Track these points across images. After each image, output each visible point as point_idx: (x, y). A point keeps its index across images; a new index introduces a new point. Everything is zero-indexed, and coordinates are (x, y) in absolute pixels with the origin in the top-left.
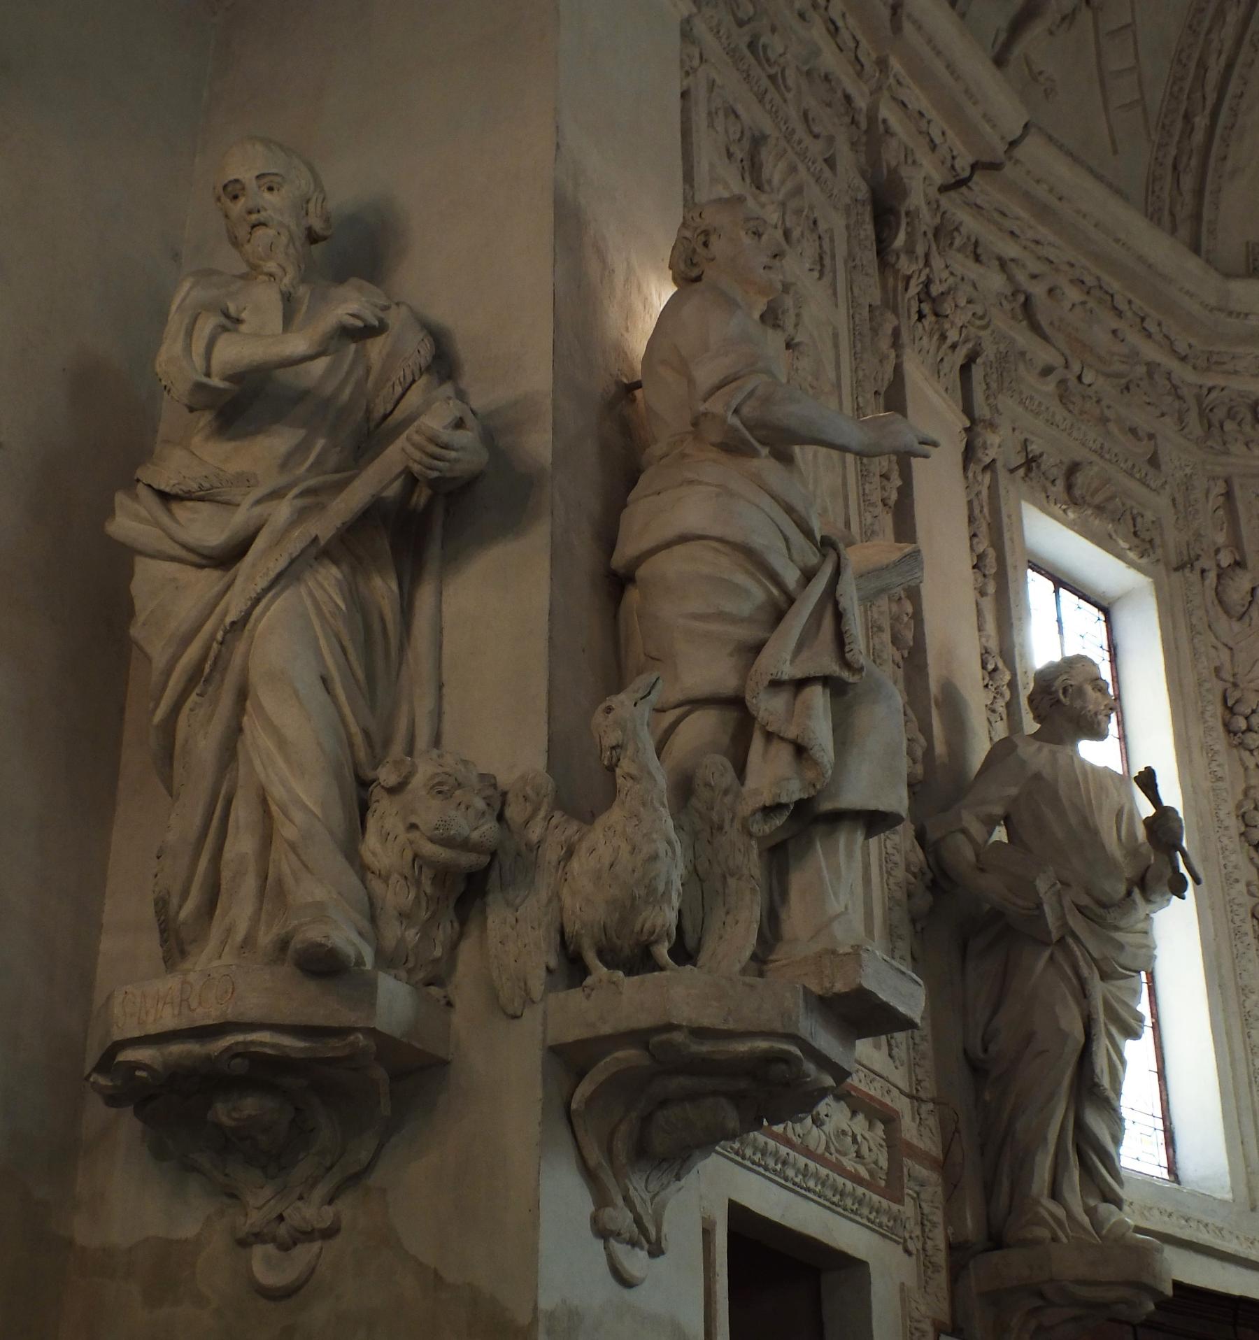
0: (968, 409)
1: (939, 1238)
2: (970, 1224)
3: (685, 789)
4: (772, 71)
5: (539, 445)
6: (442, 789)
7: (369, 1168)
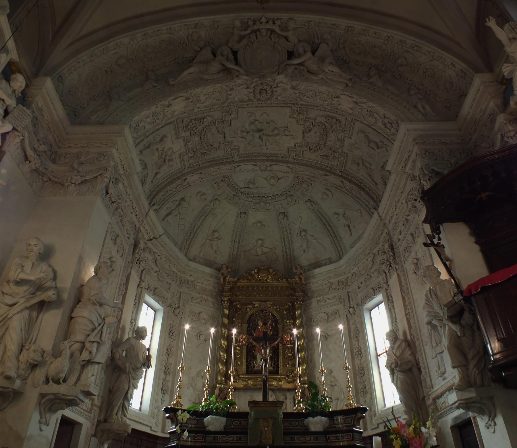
0: (141, 279)
2: (102, 418)
3: (72, 355)
5: (65, 296)
6: (34, 351)
7: (5, 409)
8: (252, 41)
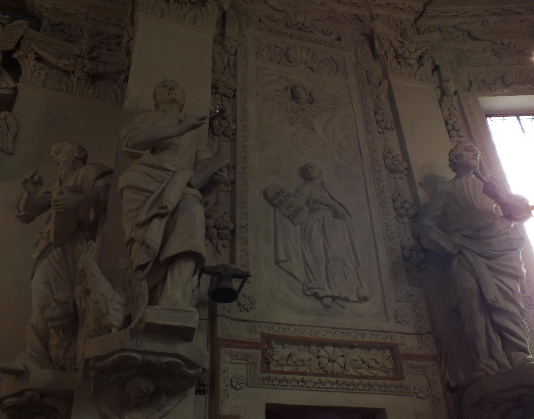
1: (439, 387)
4: (298, 26)
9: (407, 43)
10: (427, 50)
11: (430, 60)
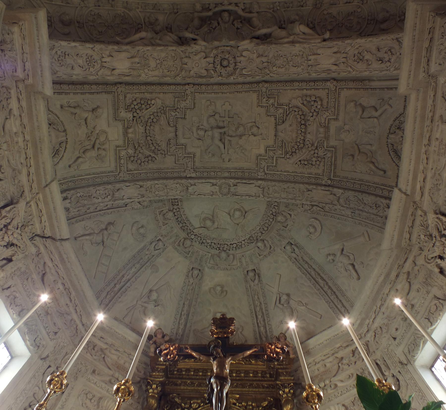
8: (214, 27)
9: (19, 231)
10: (19, 247)
11: (13, 252)
